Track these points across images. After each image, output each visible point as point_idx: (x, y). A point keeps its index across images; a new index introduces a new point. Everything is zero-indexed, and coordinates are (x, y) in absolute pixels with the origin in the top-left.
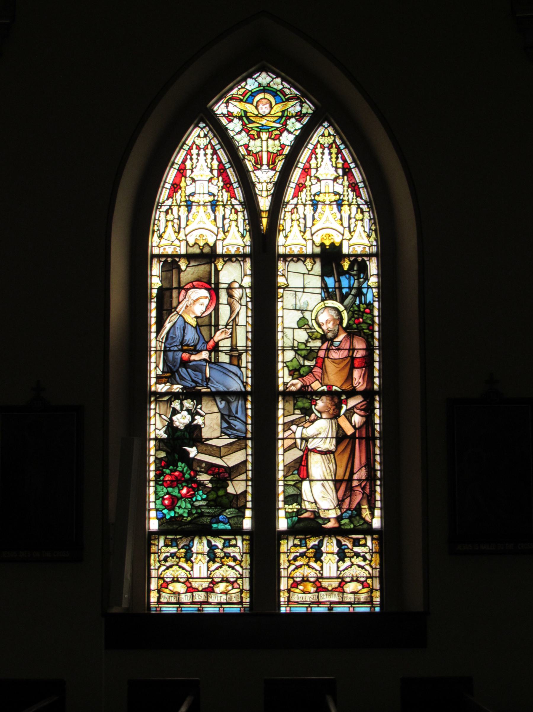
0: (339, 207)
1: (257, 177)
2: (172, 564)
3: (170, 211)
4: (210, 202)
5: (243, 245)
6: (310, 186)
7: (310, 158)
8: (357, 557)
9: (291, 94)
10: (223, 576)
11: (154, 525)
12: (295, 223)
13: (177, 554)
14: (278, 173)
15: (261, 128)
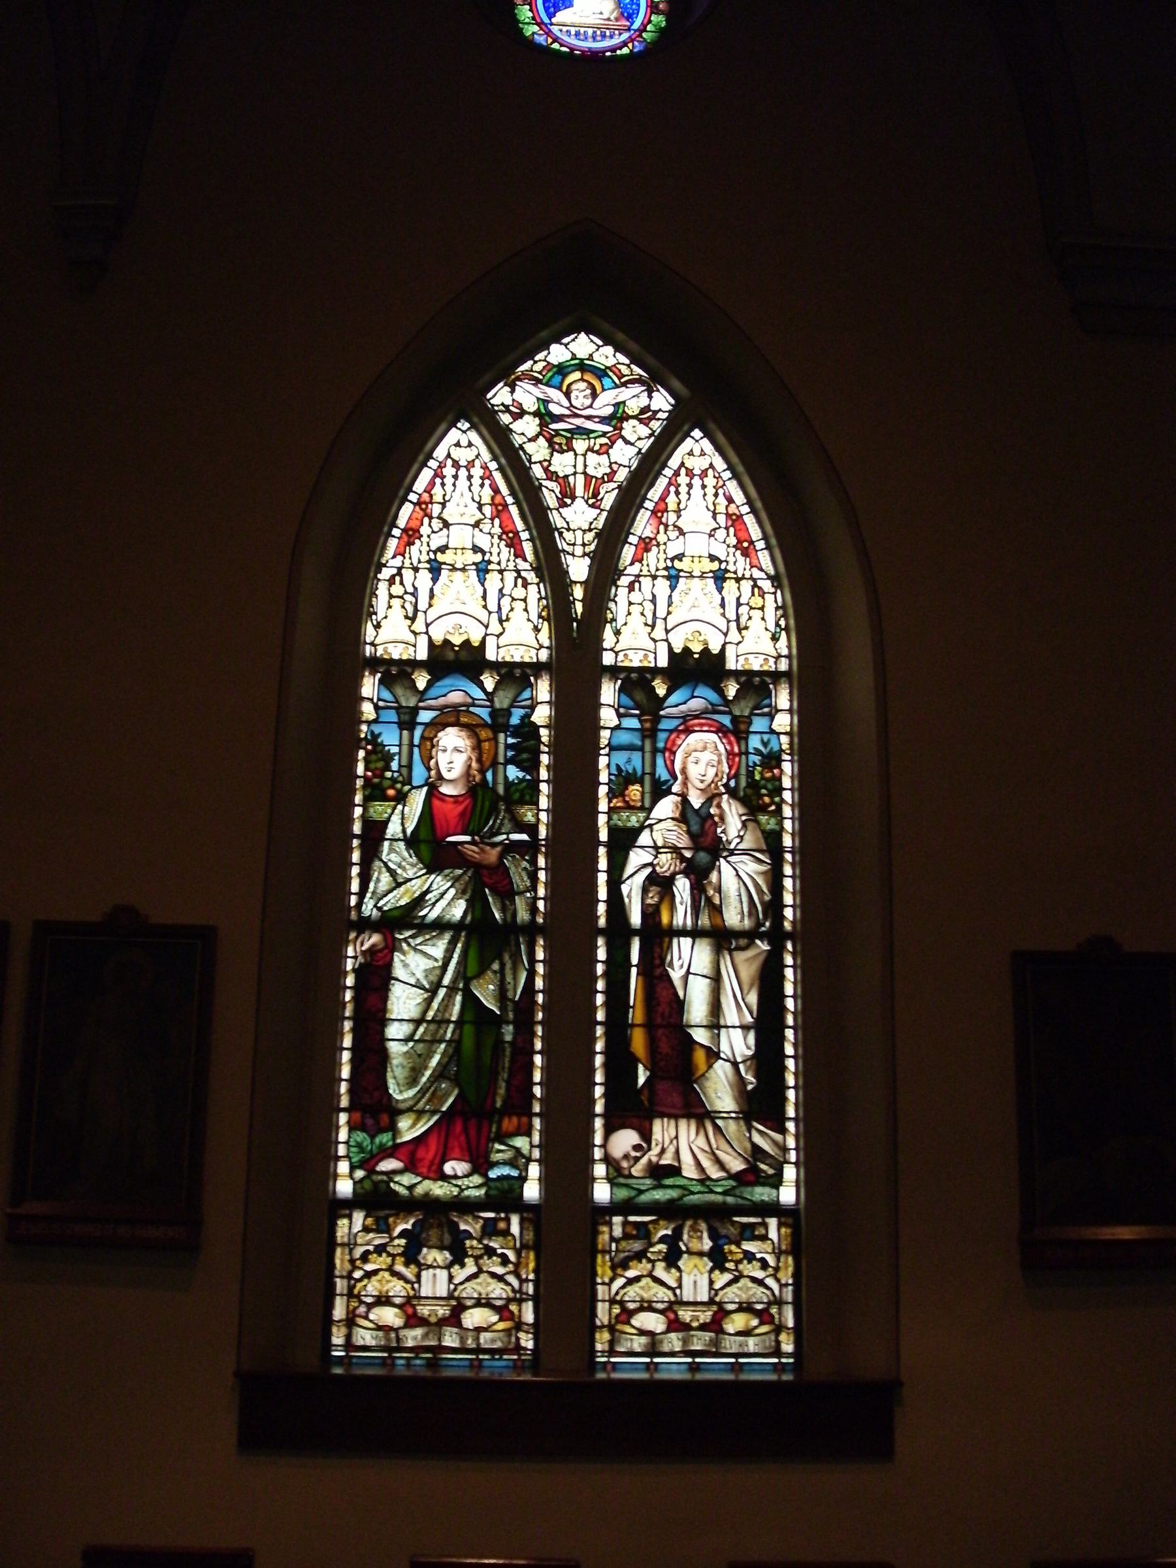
0: (719, 582)
1: (564, 519)
2: (378, 1267)
3: (398, 579)
4: (474, 564)
5: (775, 654)
6: (665, 544)
7: (432, 484)
8: (490, 1258)
9: (632, 375)
10: (480, 1294)
11: (344, 1188)
12: (396, 603)
13: (389, 1249)
14: (605, 514)
15: (575, 431)
